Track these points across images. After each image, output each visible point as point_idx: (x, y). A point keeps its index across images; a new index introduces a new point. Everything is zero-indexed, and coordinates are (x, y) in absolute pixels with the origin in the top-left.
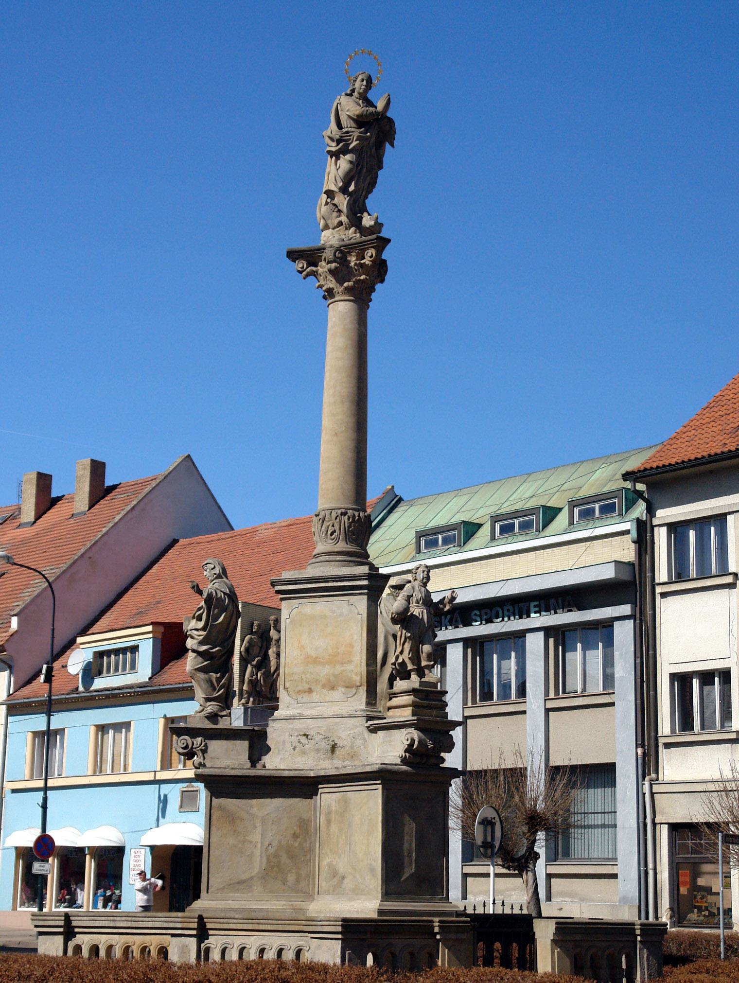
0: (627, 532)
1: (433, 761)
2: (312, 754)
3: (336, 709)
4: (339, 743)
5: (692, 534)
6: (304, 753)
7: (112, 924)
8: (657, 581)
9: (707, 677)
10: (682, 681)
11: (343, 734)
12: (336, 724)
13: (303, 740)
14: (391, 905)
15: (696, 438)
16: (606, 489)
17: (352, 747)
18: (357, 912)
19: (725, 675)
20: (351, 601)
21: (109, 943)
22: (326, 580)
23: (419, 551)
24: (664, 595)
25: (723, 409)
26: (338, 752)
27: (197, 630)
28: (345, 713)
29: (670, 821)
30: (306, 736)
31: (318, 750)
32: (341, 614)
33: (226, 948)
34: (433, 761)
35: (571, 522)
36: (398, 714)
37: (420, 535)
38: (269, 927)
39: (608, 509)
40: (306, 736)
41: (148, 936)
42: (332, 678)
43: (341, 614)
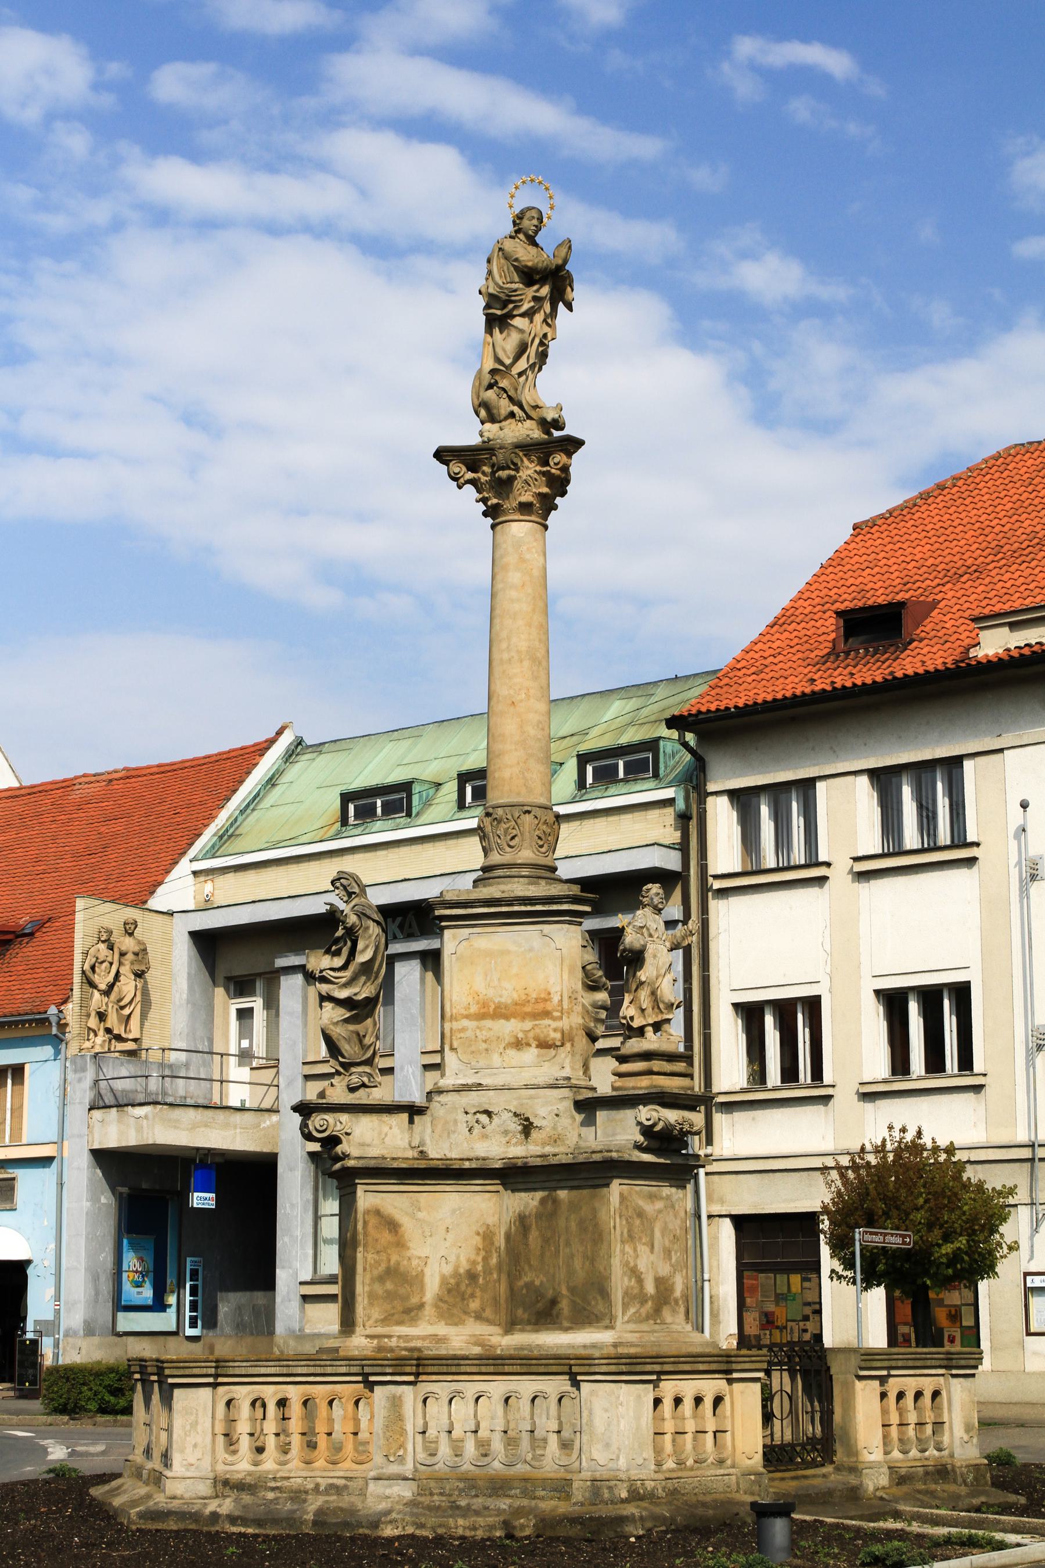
0: (670, 802)
1: (675, 1146)
2: (498, 1136)
3: (528, 1076)
4: (536, 1122)
5: (765, 810)
6: (485, 1137)
7: (285, 1371)
8: (711, 871)
9: (785, 1010)
10: (750, 1014)
11: (542, 1111)
12: (531, 1098)
13: (484, 1118)
14: (752, 1338)
15: (767, 670)
16: (624, 740)
17: (554, 1128)
18: (585, 1347)
19: (813, 1005)
20: (545, 932)
21: (279, 1396)
22: (510, 902)
23: (344, 821)
24: (723, 893)
25: (799, 628)
26: (534, 1134)
27: (332, 969)
28: (541, 1080)
29: (733, 1213)
30: (488, 1113)
31: (506, 1132)
32: (531, 950)
33: (509, 1397)
34: (675, 1146)
35: (581, 783)
36: (631, 1085)
37: (346, 798)
38: (542, 1369)
39: (636, 770)
40: (488, 1113)
41: (338, 1386)
42: (520, 1035)
43: (531, 950)
